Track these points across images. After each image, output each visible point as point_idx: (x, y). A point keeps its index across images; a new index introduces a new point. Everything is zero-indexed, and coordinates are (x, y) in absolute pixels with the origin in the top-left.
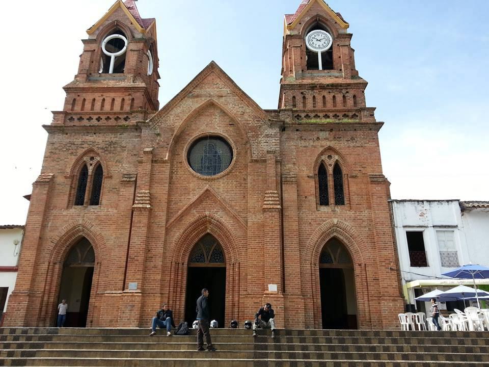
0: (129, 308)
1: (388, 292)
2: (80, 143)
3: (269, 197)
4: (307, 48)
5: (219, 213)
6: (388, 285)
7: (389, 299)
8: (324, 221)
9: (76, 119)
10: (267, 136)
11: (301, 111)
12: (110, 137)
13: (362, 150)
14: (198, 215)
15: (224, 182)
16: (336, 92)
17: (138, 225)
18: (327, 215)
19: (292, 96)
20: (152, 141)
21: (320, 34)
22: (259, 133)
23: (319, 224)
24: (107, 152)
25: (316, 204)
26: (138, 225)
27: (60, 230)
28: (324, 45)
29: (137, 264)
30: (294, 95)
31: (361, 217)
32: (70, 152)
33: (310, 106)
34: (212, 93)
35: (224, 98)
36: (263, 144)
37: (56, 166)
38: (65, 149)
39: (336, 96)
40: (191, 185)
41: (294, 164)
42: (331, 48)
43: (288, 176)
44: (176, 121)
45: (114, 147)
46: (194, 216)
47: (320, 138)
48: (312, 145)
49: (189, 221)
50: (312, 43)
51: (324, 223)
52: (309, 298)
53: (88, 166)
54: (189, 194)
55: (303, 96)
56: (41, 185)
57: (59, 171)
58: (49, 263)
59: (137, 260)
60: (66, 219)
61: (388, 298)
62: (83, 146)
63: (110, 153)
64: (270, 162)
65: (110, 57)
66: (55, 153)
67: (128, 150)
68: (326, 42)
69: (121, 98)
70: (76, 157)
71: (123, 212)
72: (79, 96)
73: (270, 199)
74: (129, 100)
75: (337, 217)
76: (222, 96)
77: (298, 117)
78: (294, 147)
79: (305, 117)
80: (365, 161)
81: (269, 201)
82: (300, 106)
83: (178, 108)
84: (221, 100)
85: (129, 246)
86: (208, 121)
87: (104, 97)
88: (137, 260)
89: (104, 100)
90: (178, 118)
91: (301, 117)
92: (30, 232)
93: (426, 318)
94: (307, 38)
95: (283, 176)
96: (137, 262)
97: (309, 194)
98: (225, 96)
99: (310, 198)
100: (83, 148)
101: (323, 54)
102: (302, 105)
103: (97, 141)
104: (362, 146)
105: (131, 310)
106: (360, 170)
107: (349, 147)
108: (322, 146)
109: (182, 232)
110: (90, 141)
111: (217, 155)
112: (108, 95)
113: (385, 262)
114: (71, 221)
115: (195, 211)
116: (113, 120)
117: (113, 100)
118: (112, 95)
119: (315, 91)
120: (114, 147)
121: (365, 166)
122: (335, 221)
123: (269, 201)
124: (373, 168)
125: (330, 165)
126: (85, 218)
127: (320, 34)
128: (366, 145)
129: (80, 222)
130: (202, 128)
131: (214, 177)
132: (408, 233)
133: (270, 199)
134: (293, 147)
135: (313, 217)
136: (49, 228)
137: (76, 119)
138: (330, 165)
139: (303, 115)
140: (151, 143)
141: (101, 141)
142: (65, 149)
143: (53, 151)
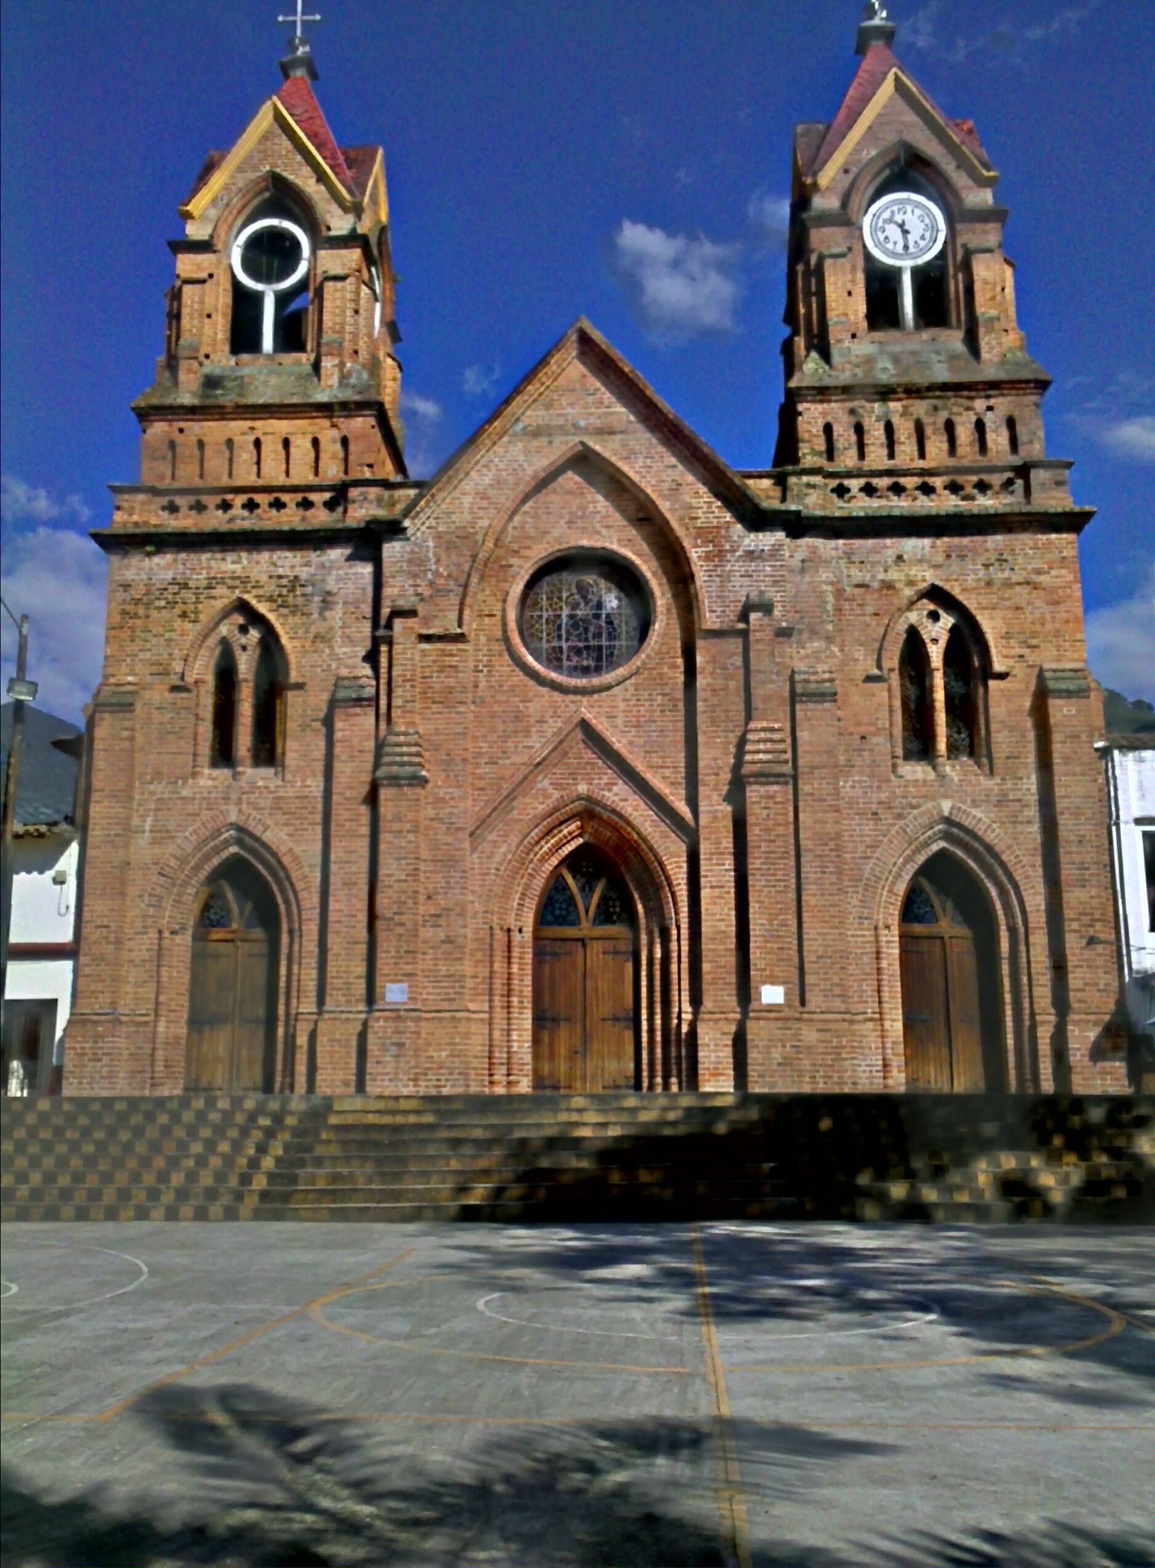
0: (394, 1050)
1: (1085, 1002)
2: (205, 583)
3: (759, 741)
4: (868, 257)
5: (615, 789)
6: (1086, 984)
7: (1088, 1022)
8: (913, 807)
9: (211, 507)
10: (750, 555)
11: (849, 475)
12: (288, 562)
13: (1030, 593)
14: (556, 795)
15: (628, 696)
16: (955, 409)
17: (396, 826)
18: (924, 790)
19: (821, 423)
20: (415, 576)
21: (909, 208)
22: (727, 547)
23: (900, 816)
24: (284, 611)
25: (894, 757)
26: (396, 826)
27: (179, 841)
28: (922, 243)
29: (401, 935)
30: (829, 419)
31: (1019, 795)
32: (178, 610)
33: (877, 457)
34: (582, 423)
35: (618, 437)
36: (737, 581)
37: (141, 655)
38: (163, 603)
39: (956, 419)
40: (533, 708)
41: (829, 639)
42: (942, 254)
43: (812, 678)
44: (481, 513)
45: (304, 595)
46: (547, 796)
47: (906, 557)
48: (883, 581)
49: (533, 812)
50: (881, 237)
51: (915, 812)
52: (872, 1020)
53: (238, 652)
54: (527, 733)
55: (853, 420)
56: (112, 712)
57: (154, 669)
58: (160, 932)
59: (402, 924)
60: (190, 808)
61: (1083, 1017)
62: (214, 592)
63: (293, 613)
64: (758, 635)
65: (258, 297)
66: (135, 616)
67: (345, 603)
68: (927, 235)
69: (309, 438)
70: (198, 626)
71: (351, 788)
72: (181, 430)
73: (762, 746)
74: (334, 441)
75: (952, 797)
76: (612, 433)
77: (841, 491)
78: (830, 588)
79: (862, 490)
80: (1038, 627)
81: (758, 752)
82: (848, 459)
83: (485, 471)
84: (611, 445)
85: (372, 917)
86: (574, 508)
87: (258, 434)
88: (402, 924)
89: (258, 443)
90: (485, 503)
91: (848, 490)
92: (99, 847)
93: (170, 337)
94: (867, 221)
95: (797, 677)
96: (400, 930)
97: (873, 729)
98: (621, 432)
99: (876, 740)
100: (214, 598)
101: (917, 272)
102: (853, 452)
103: (254, 575)
104: (1028, 583)
105: (398, 1056)
106: (1022, 656)
107: (989, 584)
108: (911, 583)
109: (514, 844)
110: (233, 578)
111: (604, 612)
112: (270, 430)
113: (1078, 920)
114: (205, 815)
115: (546, 782)
116: (237, 511)
117: (286, 443)
118: (282, 426)
119: (892, 405)
120: (304, 595)
121: (1034, 642)
122: (946, 806)
123: (758, 752)
124: (1058, 649)
125: (935, 641)
126: (244, 806)
127: (909, 208)
128: (1042, 578)
129: (233, 817)
130: (556, 533)
131: (596, 681)
132: (1145, 835)
133: (762, 746)
134: (825, 587)
135: (883, 796)
136: (147, 834)
137: (292, 506)
138: (935, 641)
139: (854, 484)
140: (411, 582)
141: (264, 578)
142: (163, 603)
143: (128, 608)
